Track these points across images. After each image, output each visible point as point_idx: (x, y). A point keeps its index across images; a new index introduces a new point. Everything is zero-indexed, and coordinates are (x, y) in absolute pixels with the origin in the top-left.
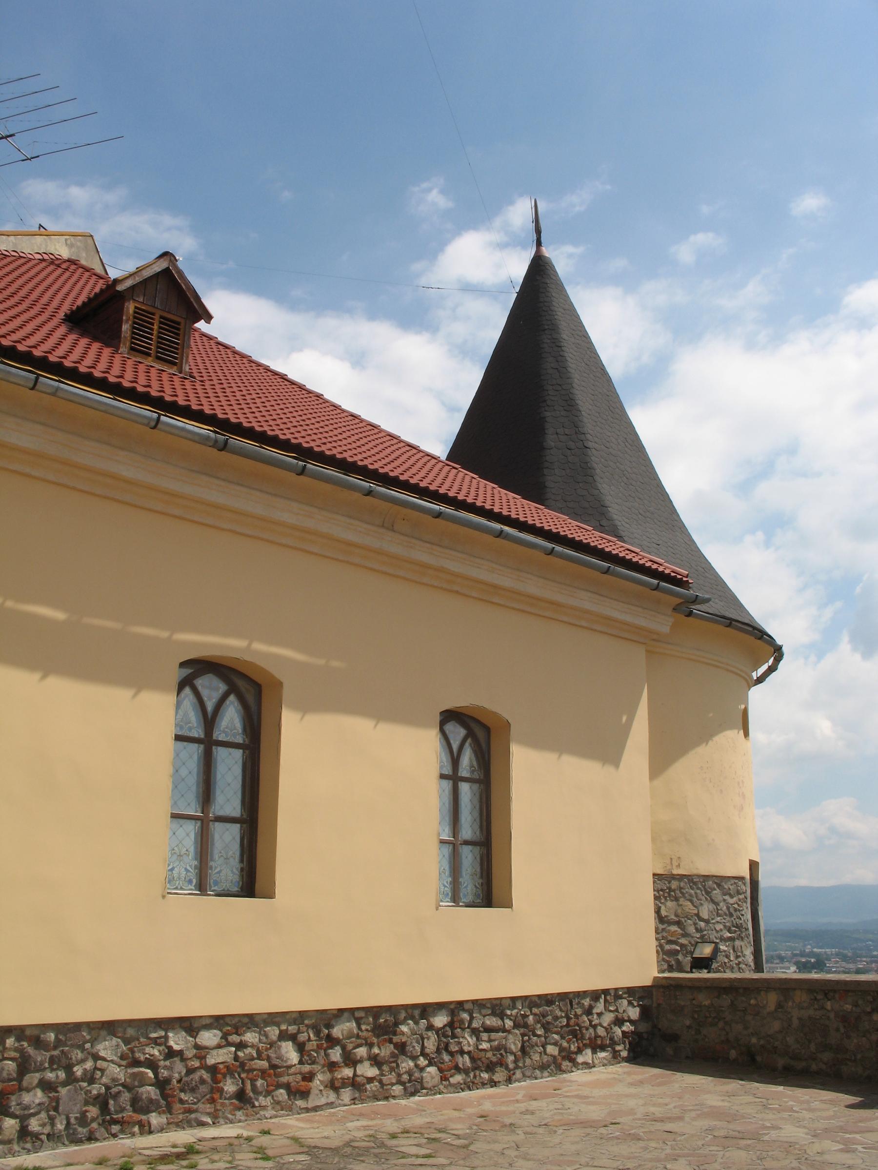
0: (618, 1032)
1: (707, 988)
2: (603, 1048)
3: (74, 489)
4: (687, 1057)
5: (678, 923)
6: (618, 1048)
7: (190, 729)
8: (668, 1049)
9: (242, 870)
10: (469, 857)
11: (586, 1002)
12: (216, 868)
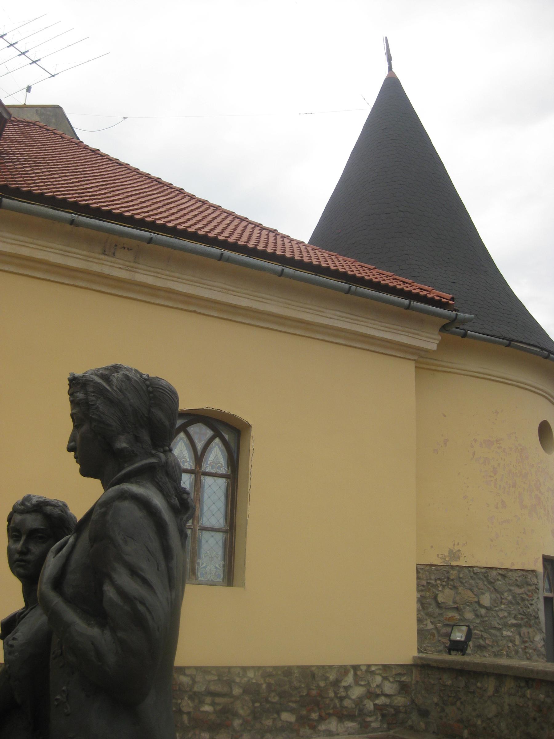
0: (369, 705)
2: (351, 717)
3: (295, 334)
4: (434, 732)
5: (457, 609)
6: (369, 719)
8: (421, 723)
9: (224, 566)
12: (203, 564)
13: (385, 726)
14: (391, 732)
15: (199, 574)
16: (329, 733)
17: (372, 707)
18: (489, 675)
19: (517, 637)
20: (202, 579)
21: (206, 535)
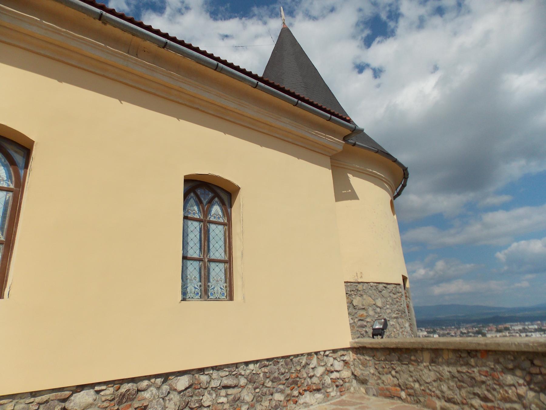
1: (381, 349)
2: (318, 390)
4: (374, 395)
6: (328, 390)
7: (219, 218)
10: (193, 268)
11: (304, 361)
13: (338, 394)
14: (343, 398)
15: (209, 294)
16: (306, 405)
17: (330, 381)
18: (422, 350)
19: (398, 325)
20: (212, 297)
21: (213, 265)
